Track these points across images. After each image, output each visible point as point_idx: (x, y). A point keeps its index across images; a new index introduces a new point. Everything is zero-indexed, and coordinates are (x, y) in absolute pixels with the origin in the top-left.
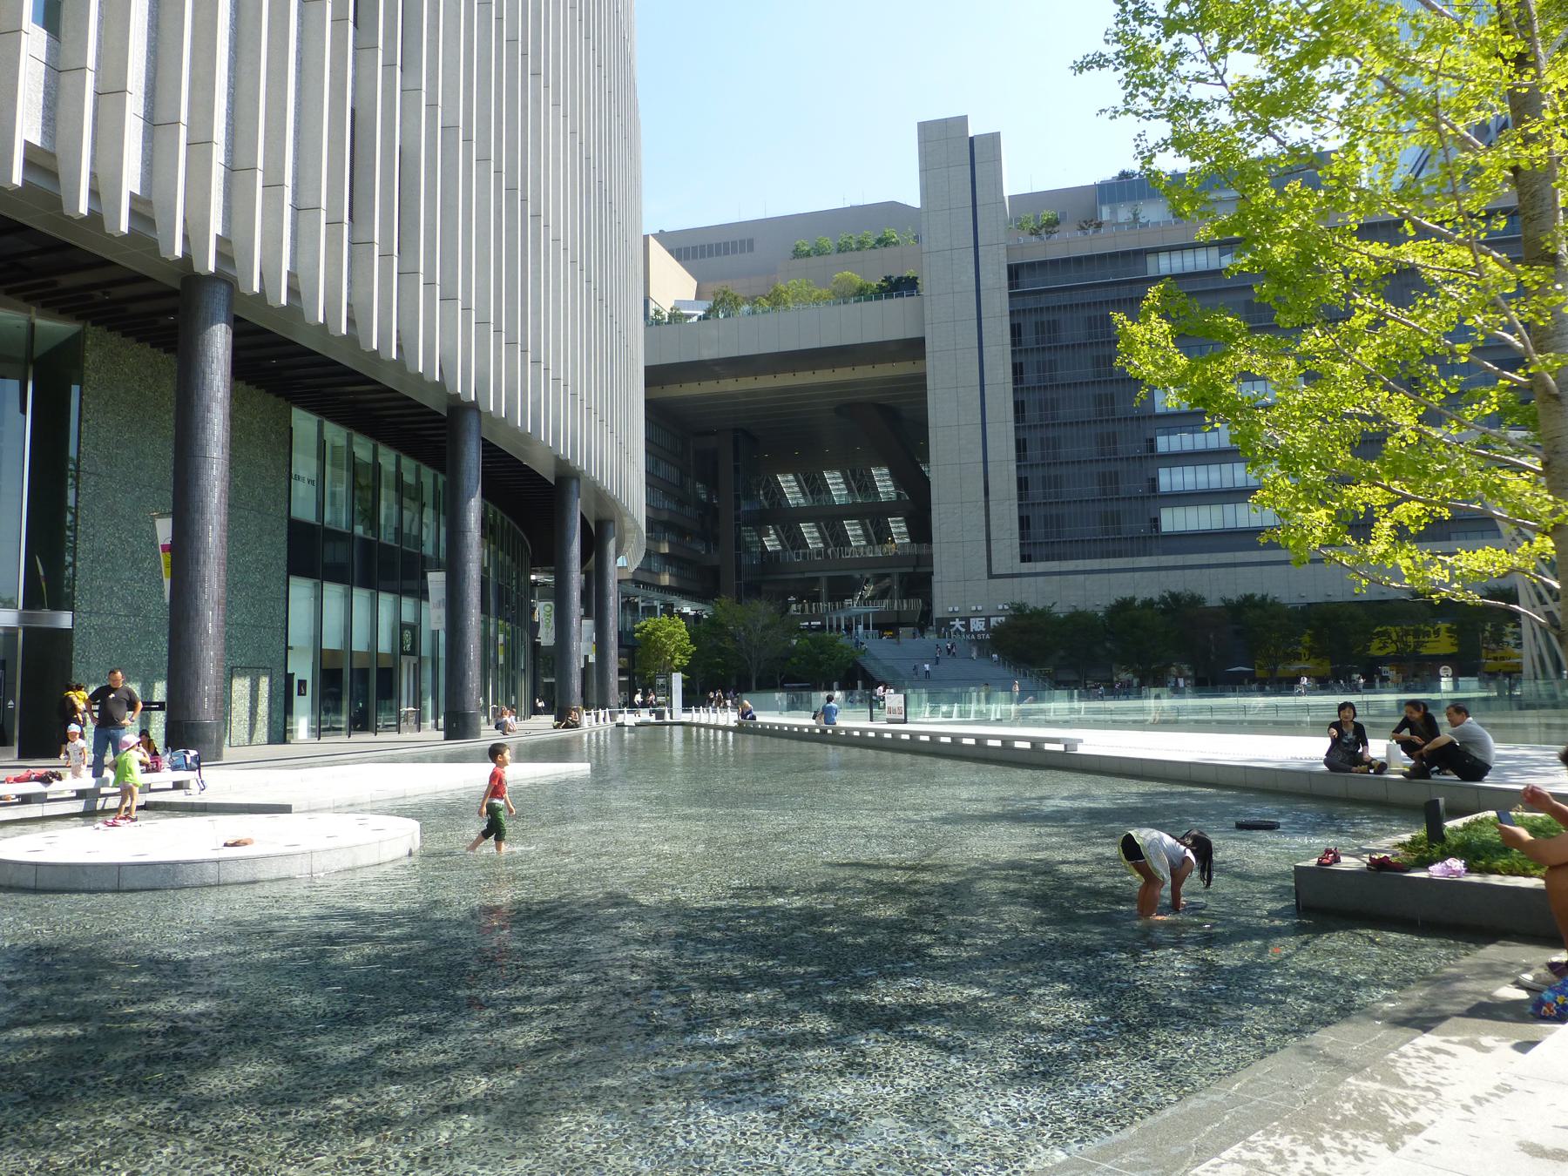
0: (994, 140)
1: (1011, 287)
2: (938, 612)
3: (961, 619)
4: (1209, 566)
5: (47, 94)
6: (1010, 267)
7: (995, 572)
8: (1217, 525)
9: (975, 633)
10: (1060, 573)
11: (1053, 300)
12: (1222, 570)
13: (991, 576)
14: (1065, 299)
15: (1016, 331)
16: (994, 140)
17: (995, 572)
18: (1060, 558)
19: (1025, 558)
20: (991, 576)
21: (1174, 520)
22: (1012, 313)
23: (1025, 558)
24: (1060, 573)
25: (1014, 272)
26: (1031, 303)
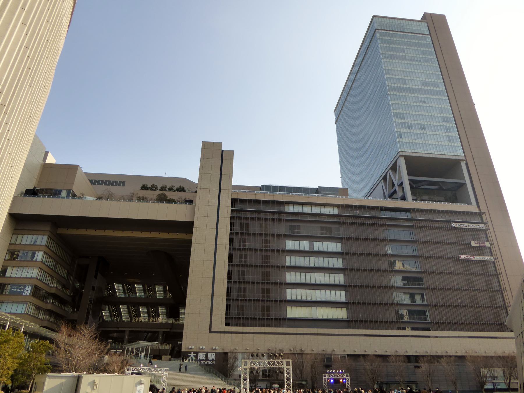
0: (231, 153)
1: (232, 207)
2: (183, 350)
3: (194, 353)
4: (307, 334)
5: (277, 187)
6: (232, 199)
7: (213, 330)
8: (309, 317)
9: (200, 360)
10: (243, 333)
11: (248, 215)
12: (302, 336)
13: (211, 332)
14: (253, 215)
15: (232, 225)
16: (231, 153)
17: (213, 330)
18: (243, 325)
19: (227, 324)
20: (211, 332)
21: (292, 312)
22: (231, 218)
23: (227, 324)
24: (243, 333)
25: (234, 202)
26: (239, 215)
